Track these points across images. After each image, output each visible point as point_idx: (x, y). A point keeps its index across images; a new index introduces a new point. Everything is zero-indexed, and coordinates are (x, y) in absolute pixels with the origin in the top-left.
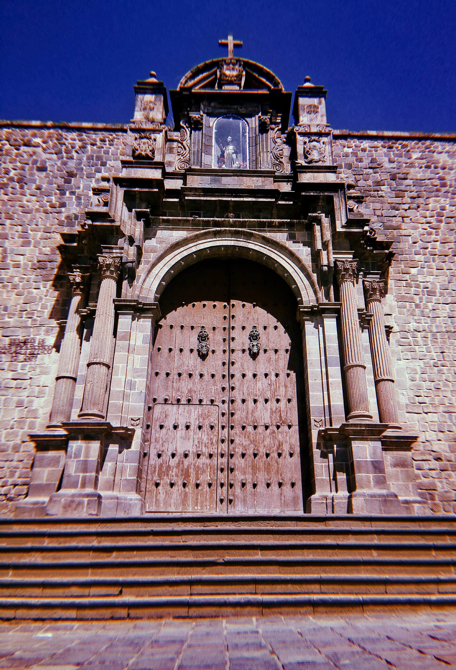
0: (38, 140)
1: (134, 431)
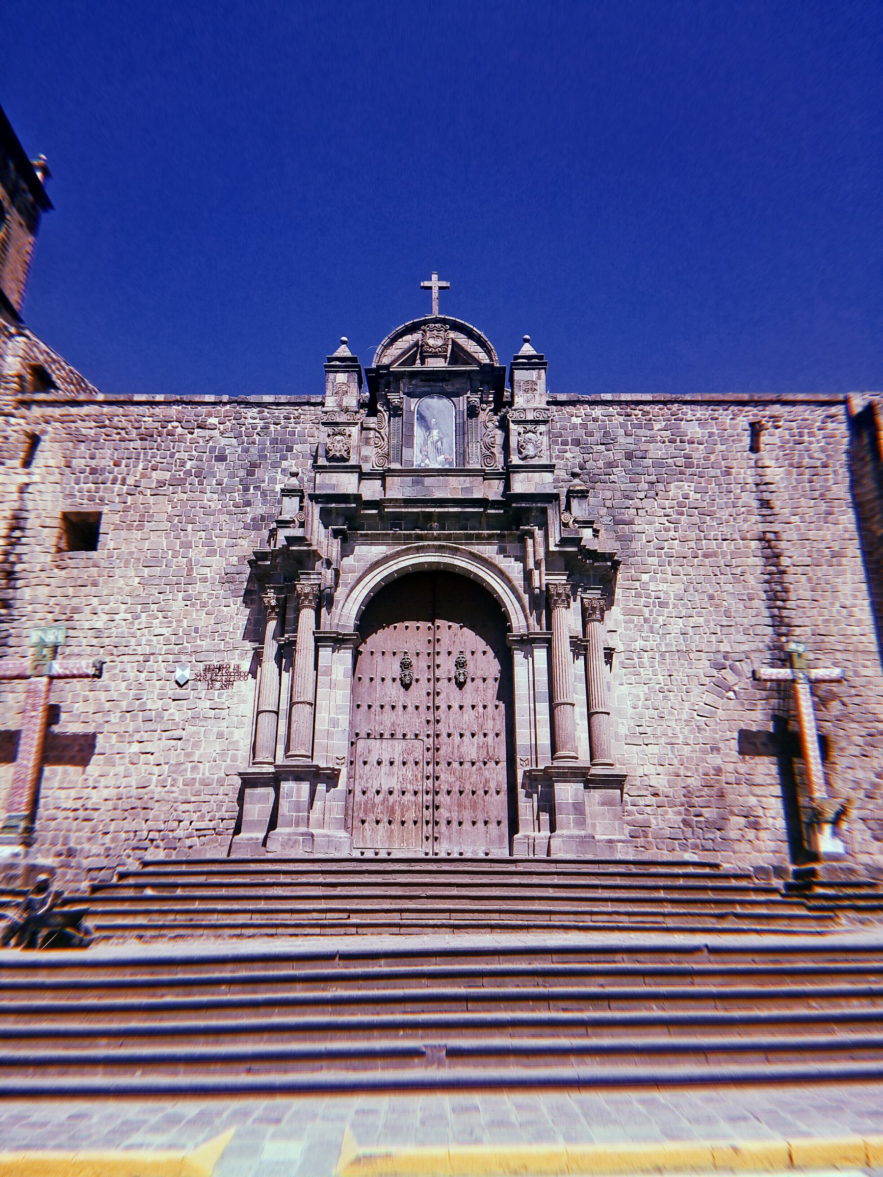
0: (213, 420)
1: (339, 770)
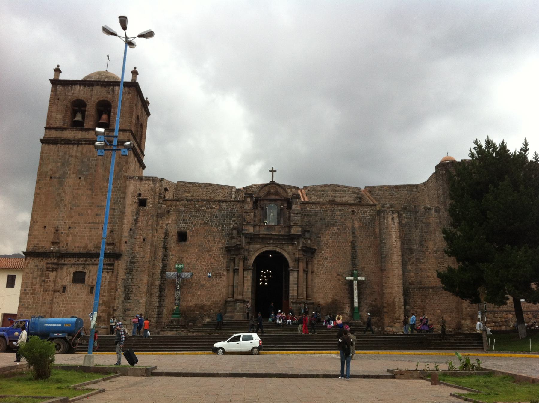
0: (214, 206)
